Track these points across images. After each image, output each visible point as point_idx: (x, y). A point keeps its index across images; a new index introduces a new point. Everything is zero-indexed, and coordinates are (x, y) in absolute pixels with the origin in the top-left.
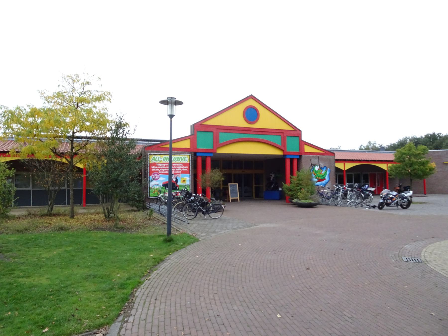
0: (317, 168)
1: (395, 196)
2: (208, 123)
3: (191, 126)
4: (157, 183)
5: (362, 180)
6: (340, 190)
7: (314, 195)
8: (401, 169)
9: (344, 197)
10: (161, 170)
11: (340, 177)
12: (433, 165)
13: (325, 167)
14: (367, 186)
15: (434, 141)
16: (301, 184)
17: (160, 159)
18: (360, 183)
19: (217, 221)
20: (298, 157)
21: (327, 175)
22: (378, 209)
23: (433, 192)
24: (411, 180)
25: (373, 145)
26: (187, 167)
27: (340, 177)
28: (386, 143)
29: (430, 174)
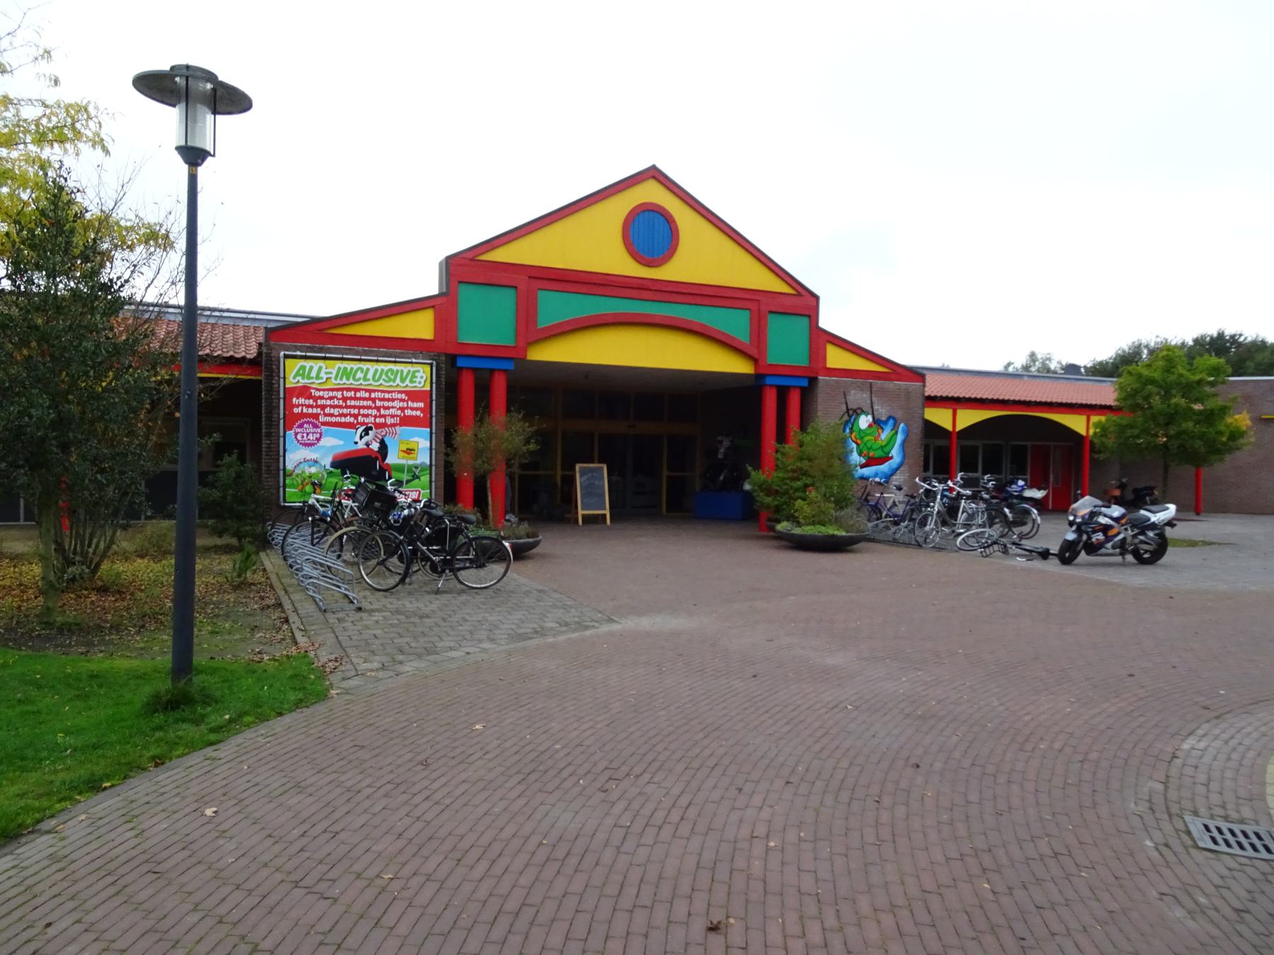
0: (864, 421)
1: (1116, 520)
2: (501, 255)
3: (441, 264)
4: (308, 456)
5: (1006, 465)
6: (935, 493)
7: (849, 511)
8: (1136, 432)
9: (947, 518)
10: (327, 411)
11: (937, 451)
12: (1242, 420)
13: (889, 418)
14: (1021, 483)
15: (1229, 354)
16: (805, 474)
17: (322, 375)
18: (999, 473)
19: (479, 598)
20: (805, 383)
21: (895, 443)
22: (1057, 561)
23: (1222, 508)
24: (1166, 468)
25: (1043, 363)
26: (421, 405)
27: (937, 451)
28: (1084, 359)
29: (1230, 450)
